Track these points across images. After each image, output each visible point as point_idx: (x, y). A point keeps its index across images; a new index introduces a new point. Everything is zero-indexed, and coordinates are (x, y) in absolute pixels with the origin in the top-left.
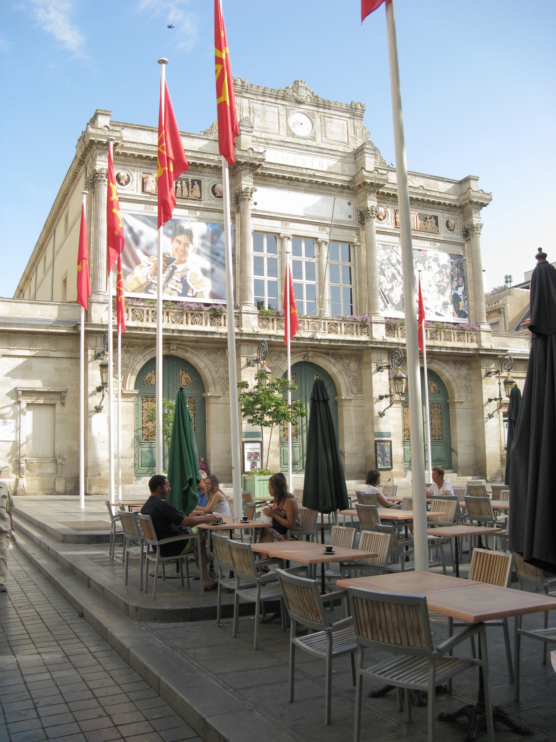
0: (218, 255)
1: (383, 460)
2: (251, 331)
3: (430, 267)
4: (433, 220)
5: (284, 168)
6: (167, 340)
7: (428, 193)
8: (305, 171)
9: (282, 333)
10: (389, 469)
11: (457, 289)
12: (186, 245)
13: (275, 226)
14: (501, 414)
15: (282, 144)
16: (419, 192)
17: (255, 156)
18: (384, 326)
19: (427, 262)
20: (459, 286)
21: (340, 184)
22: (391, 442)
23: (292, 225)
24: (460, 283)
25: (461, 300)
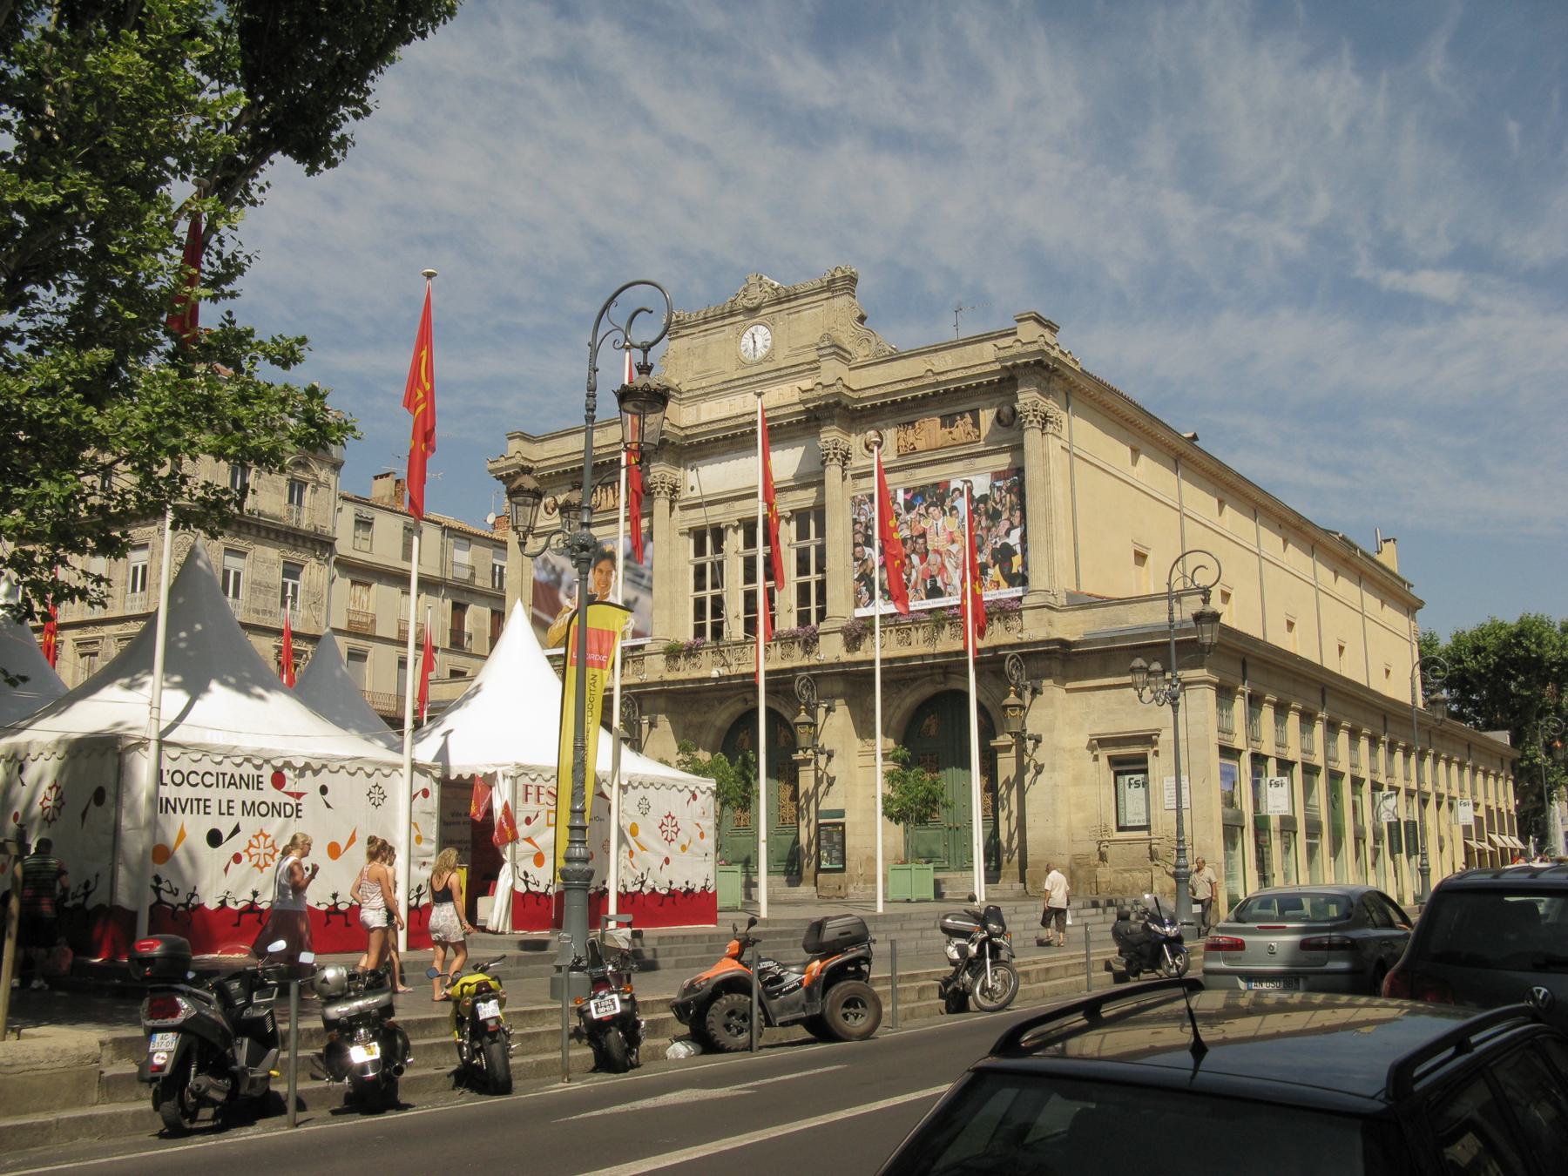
0: (642, 576)
1: (830, 854)
2: (656, 678)
3: (953, 508)
4: (968, 418)
5: (715, 426)
6: (638, 696)
7: (943, 378)
8: (741, 421)
9: (959, 646)
10: (843, 870)
11: (1008, 534)
12: (609, 573)
13: (717, 515)
14: (1103, 761)
15: (728, 387)
16: (926, 381)
17: (826, 391)
18: (839, 637)
19: (948, 501)
20: (1012, 527)
21: (1032, 360)
22: (843, 825)
23: (738, 505)
24: (1016, 521)
25: (1015, 553)
